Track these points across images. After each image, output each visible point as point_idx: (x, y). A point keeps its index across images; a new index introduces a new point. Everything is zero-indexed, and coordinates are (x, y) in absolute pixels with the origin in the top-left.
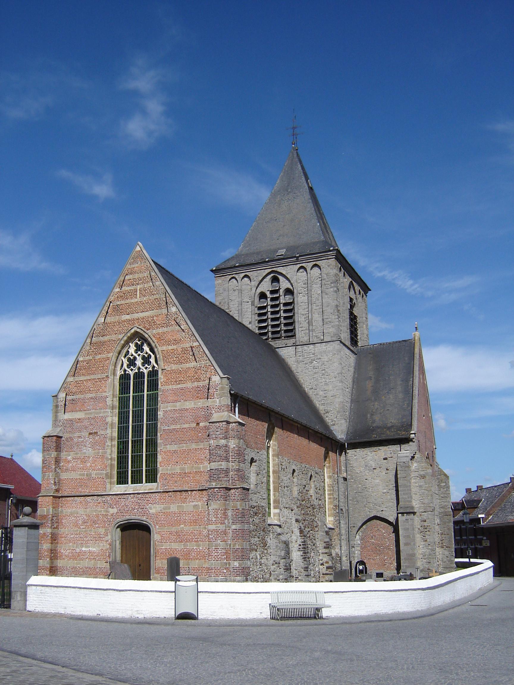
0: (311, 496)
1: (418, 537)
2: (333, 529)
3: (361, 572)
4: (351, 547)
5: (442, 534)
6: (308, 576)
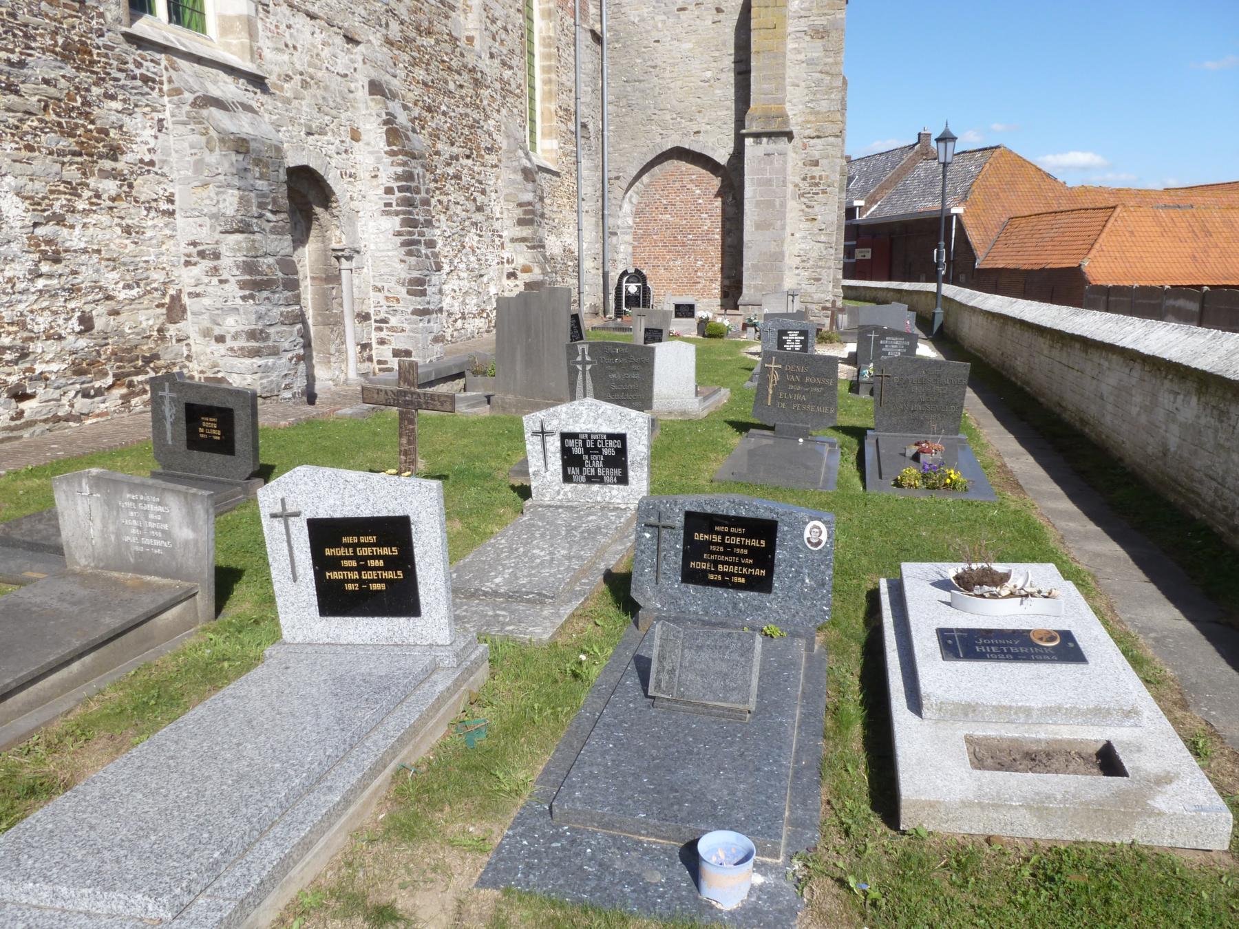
0: (470, 39)
1: (793, 207)
2: (557, 174)
3: (633, 301)
4: (606, 233)
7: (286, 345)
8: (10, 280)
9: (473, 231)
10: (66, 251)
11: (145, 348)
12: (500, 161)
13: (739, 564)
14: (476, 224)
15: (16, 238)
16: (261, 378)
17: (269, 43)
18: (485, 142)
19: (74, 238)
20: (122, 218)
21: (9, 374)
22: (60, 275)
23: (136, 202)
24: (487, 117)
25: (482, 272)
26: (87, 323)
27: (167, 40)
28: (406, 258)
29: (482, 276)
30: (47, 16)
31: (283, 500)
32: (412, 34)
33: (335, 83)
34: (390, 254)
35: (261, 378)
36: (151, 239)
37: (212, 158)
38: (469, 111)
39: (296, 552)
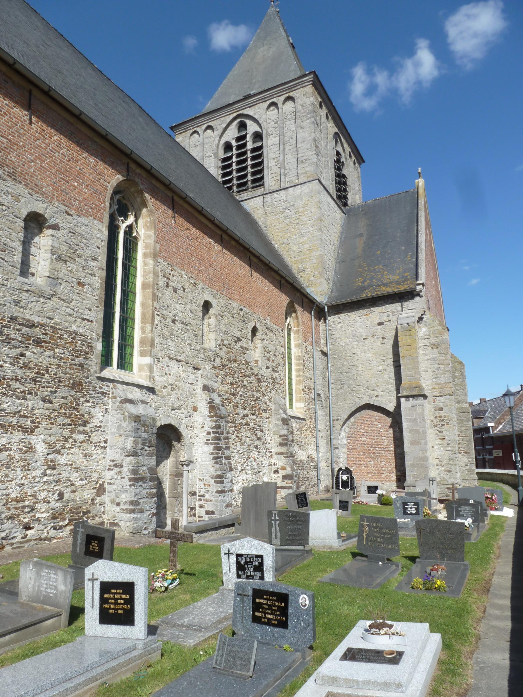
0: (256, 361)
1: (431, 433)
2: (304, 420)
3: (345, 484)
4: (332, 448)
6: (222, 492)
7: (148, 508)
8: (34, 477)
9: (255, 450)
10: (58, 465)
11: (84, 507)
12: (271, 415)
13: (274, 614)
14: (257, 446)
15: (39, 460)
16: (133, 524)
17: (158, 374)
18: (263, 407)
19: (62, 459)
20: (84, 450)
21: (25, 518)
22: (54, 475)
23: (91, 443)
24: (264, 395)
25: (259, 470)
26: (61, 495)
27: (114, 377)
28: (215, 465)
29: (259, 472)
30: (68, 373)
31: (93, 573)
32: (226, 362)
34: (207, 463)
35: (133, 524)
36: (95, 459)
37: (124, 424)
38: (254, 393)
39: (95, 595)
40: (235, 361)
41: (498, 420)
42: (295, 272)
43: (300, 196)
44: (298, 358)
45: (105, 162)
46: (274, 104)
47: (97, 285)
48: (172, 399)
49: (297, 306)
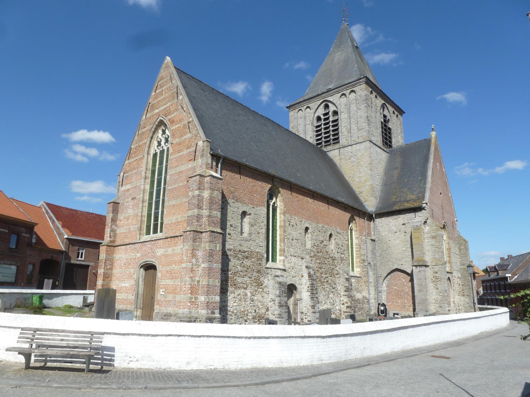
0: (332, 250)
1: (431, 286)
3: (382, 312)
4: (378, 292)
5: (463, 285)
18: (336, 272)
19: (255, 298)
24: (336, 267)
26: (255, 311)
33: (299, 267)
37: (276, 285)
40: (321, 252)
41: (514, 272)
42: (357, 193)
43: (359, 150)
44: (356, 245)
45: (264, 182)
46: (343, 94)
47: (264, 232)
48: (293, 273)
49: (355, 217)
